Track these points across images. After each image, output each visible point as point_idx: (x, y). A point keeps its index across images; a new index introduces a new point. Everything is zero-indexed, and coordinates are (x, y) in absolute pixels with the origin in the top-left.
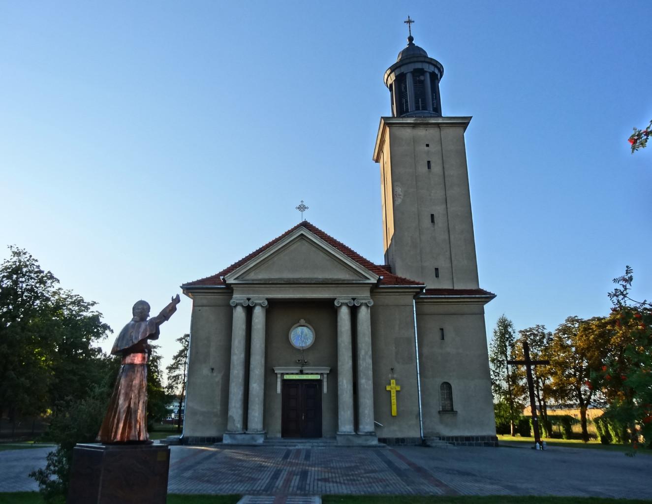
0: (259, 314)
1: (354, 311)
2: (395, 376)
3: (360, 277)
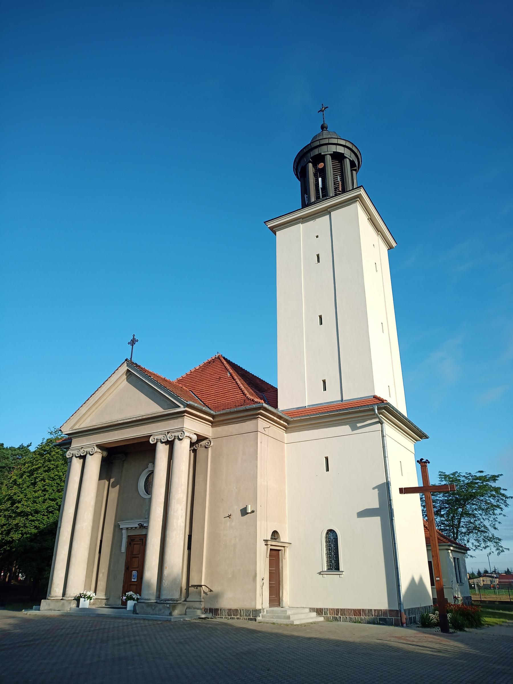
1: (171, 444)
2: (233, 524)
3: (64, 440)
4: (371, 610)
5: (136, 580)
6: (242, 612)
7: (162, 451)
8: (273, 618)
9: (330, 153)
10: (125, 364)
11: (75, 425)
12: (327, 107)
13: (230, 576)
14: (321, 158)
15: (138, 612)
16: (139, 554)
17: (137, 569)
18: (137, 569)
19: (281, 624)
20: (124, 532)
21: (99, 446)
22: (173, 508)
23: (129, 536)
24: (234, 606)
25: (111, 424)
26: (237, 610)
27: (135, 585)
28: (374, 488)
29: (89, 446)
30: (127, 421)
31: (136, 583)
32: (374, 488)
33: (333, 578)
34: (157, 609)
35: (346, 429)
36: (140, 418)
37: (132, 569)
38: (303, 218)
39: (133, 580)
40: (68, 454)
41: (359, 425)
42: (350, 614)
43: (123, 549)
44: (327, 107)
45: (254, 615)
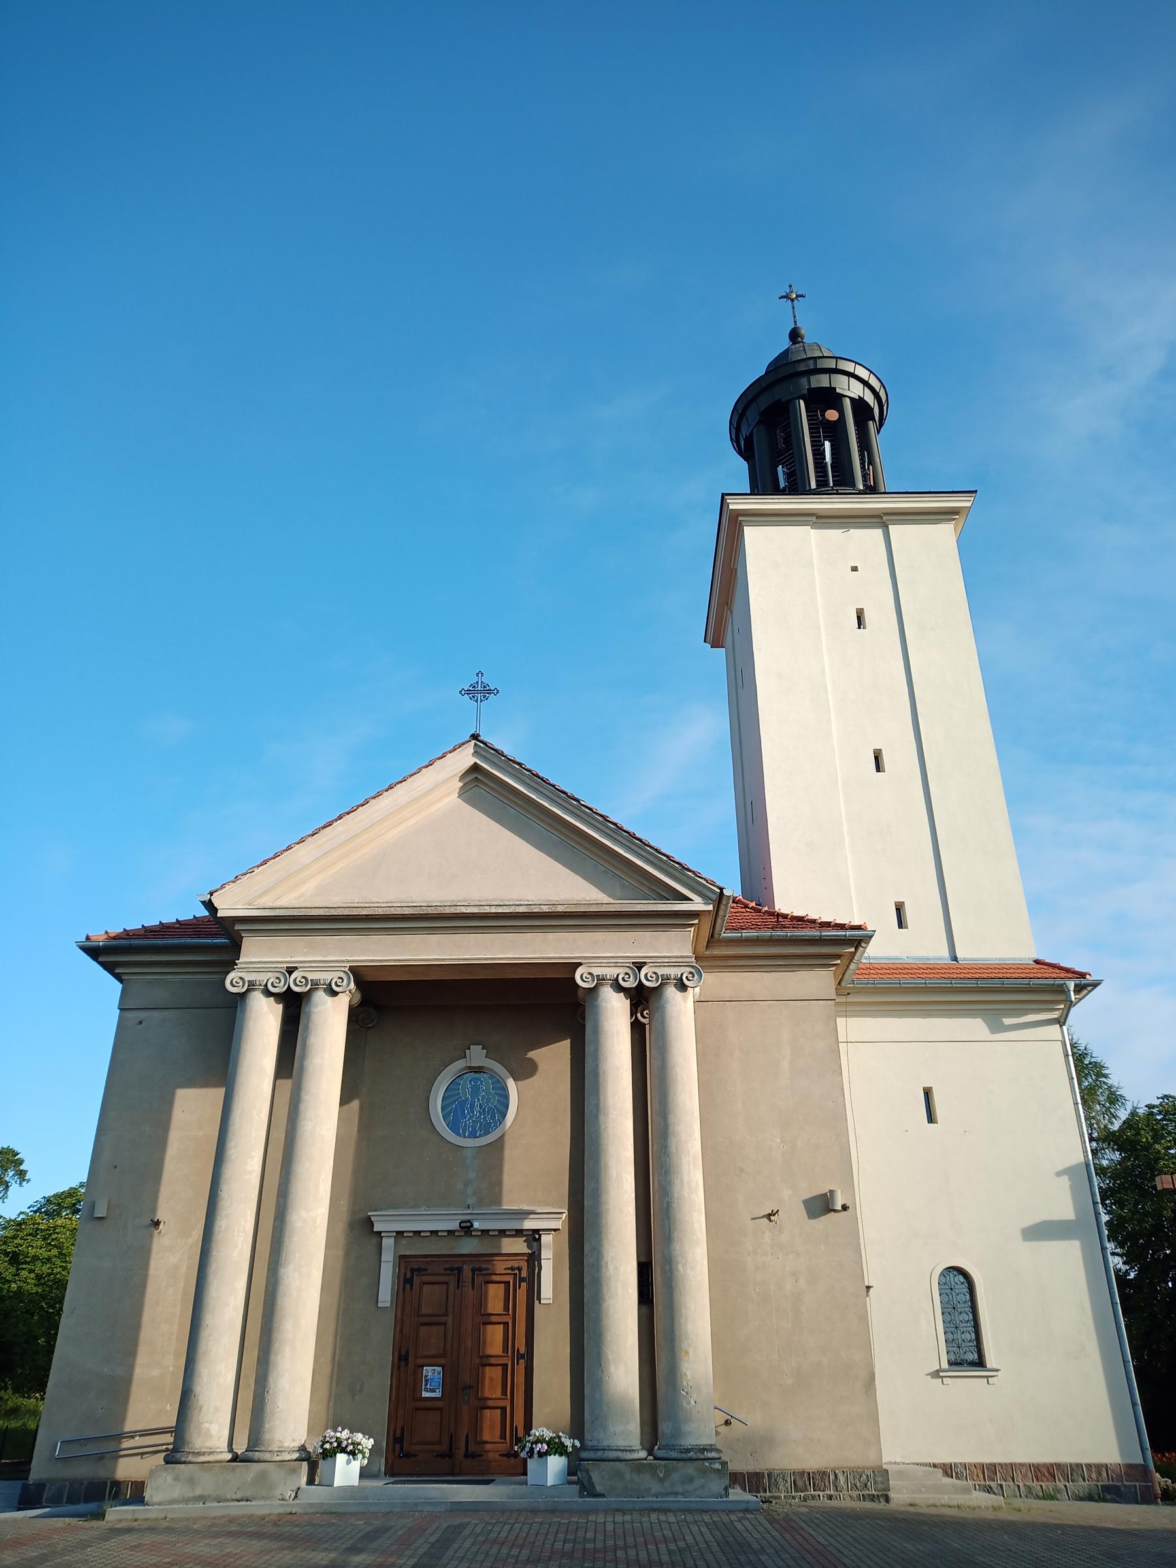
0: (330, 1022)
4: (1079, 1466)
5: (438, 1394)
6: (842, 1478)
7: (615, 1014)
8: (920, 1491)
9: (852, 395)
10: (470, 748)
11: (261, 896)
12: (802, 296)
13: (790, 1382)
14: (832, 398)
15: (599, 1488)
16: (446, 1315)
17: (442, 1361)
18: (442, 1361)
19: (263, 1518)
20: (388, 1243)
21: (357, 973)
22: (686, 1179)
23: (402, 1260)
24: (812, 1462)
25: (430, 911)
26: (823, 1474)
27: (435, 1409)
28: (1059, 1174)
29: (325, 966)
30: (464, 910)
31: (440, 1404)
32: (1059, 1174)
33: (966, 1386)
34: (675, 1477)
35: (974, 1027)
36: (545, 909)
37: (420, 1361)
38: (818, 517)
39: (425, 1394)
40: (233, 981)
41: (1008, 1021)
42: (1025, 1476)
43: (385, 1296)
44: (802, 296)
45: (880, 1486)
